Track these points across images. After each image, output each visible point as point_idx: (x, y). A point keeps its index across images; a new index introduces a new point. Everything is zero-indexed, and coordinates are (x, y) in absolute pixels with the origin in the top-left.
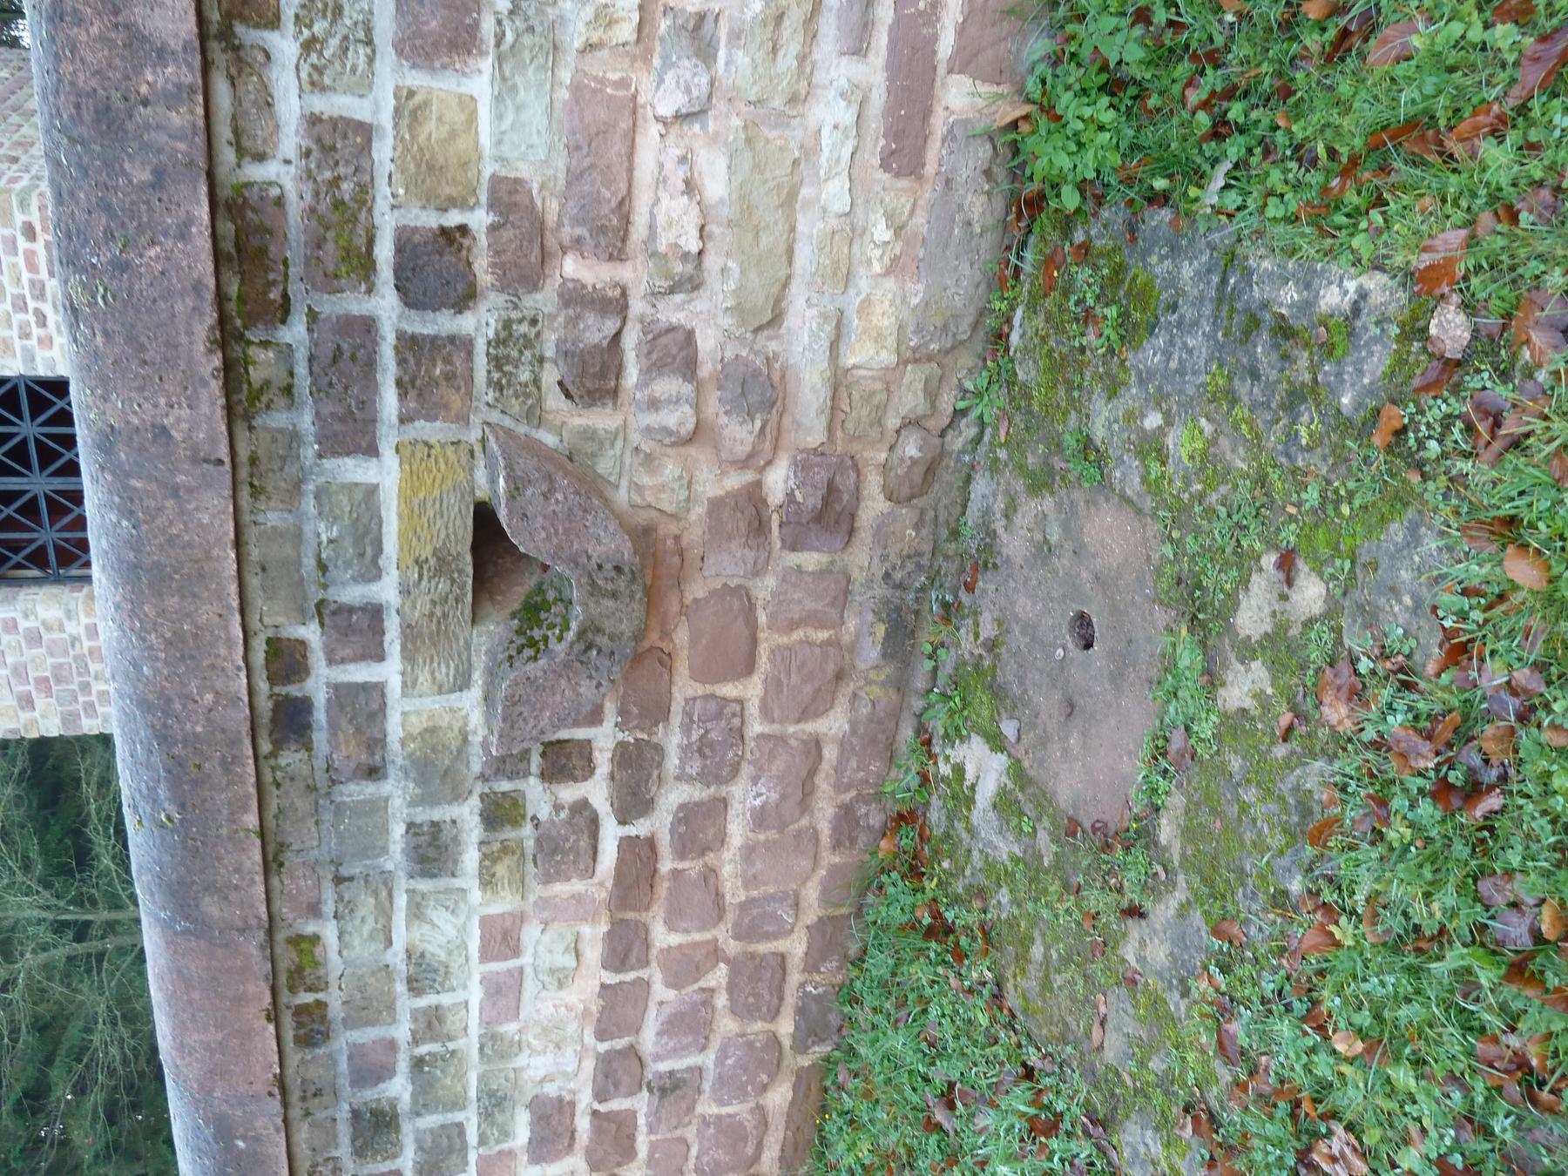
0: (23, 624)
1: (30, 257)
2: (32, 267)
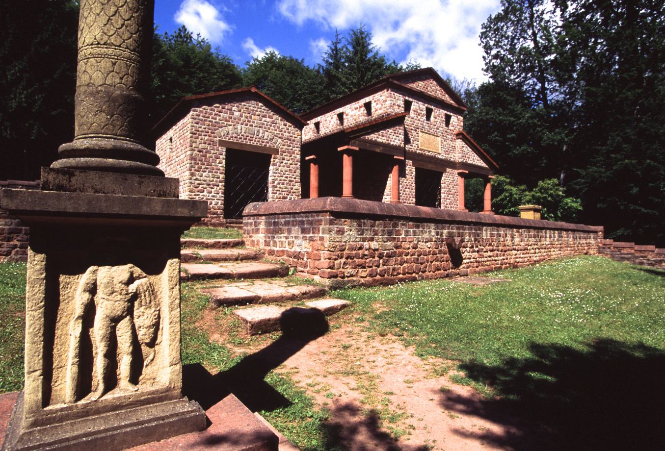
0: (221, 157)
1: (292, 178)
2: (290, 177)
